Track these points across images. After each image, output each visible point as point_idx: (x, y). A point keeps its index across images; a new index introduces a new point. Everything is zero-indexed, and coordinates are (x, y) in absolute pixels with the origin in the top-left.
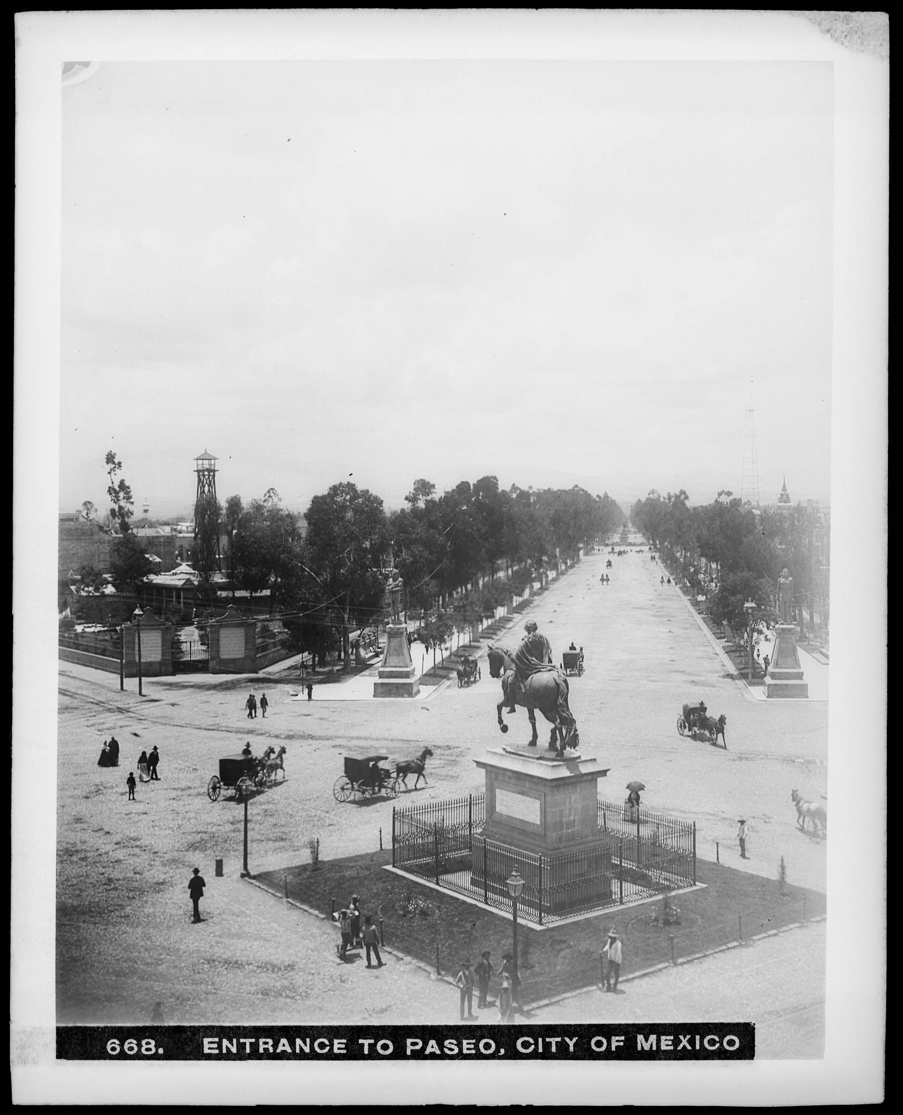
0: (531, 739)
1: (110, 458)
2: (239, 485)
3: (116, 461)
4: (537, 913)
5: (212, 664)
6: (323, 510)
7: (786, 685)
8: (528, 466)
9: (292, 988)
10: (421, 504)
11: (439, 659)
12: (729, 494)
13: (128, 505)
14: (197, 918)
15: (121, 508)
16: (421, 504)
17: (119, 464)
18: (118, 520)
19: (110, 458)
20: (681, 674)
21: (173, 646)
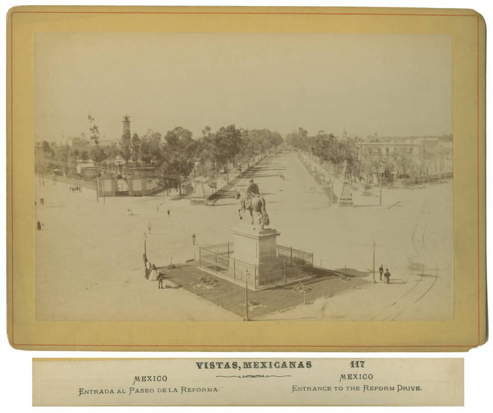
0: (317, 264)
1: (89, 117)
2: (140, 129)
3: (92, 118)
4: (248, 288)
5: (130, 193)
6: (172, 139)
7: (346, 203)
8: (245, 123)
9: (158, 280)
10: (207, 135)
11: (214, 192)
12: (323, 132)
13: (97, 134)
14: (150, 233)
15: (95, 135)
16: (207, 135)
17: (93, 119)
18: (94, 140)
19: (89, 117)
20: (263, 193)
21: (115, 186)
